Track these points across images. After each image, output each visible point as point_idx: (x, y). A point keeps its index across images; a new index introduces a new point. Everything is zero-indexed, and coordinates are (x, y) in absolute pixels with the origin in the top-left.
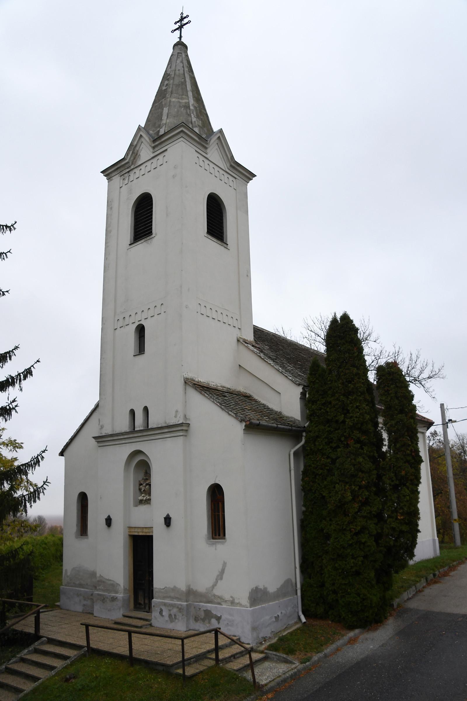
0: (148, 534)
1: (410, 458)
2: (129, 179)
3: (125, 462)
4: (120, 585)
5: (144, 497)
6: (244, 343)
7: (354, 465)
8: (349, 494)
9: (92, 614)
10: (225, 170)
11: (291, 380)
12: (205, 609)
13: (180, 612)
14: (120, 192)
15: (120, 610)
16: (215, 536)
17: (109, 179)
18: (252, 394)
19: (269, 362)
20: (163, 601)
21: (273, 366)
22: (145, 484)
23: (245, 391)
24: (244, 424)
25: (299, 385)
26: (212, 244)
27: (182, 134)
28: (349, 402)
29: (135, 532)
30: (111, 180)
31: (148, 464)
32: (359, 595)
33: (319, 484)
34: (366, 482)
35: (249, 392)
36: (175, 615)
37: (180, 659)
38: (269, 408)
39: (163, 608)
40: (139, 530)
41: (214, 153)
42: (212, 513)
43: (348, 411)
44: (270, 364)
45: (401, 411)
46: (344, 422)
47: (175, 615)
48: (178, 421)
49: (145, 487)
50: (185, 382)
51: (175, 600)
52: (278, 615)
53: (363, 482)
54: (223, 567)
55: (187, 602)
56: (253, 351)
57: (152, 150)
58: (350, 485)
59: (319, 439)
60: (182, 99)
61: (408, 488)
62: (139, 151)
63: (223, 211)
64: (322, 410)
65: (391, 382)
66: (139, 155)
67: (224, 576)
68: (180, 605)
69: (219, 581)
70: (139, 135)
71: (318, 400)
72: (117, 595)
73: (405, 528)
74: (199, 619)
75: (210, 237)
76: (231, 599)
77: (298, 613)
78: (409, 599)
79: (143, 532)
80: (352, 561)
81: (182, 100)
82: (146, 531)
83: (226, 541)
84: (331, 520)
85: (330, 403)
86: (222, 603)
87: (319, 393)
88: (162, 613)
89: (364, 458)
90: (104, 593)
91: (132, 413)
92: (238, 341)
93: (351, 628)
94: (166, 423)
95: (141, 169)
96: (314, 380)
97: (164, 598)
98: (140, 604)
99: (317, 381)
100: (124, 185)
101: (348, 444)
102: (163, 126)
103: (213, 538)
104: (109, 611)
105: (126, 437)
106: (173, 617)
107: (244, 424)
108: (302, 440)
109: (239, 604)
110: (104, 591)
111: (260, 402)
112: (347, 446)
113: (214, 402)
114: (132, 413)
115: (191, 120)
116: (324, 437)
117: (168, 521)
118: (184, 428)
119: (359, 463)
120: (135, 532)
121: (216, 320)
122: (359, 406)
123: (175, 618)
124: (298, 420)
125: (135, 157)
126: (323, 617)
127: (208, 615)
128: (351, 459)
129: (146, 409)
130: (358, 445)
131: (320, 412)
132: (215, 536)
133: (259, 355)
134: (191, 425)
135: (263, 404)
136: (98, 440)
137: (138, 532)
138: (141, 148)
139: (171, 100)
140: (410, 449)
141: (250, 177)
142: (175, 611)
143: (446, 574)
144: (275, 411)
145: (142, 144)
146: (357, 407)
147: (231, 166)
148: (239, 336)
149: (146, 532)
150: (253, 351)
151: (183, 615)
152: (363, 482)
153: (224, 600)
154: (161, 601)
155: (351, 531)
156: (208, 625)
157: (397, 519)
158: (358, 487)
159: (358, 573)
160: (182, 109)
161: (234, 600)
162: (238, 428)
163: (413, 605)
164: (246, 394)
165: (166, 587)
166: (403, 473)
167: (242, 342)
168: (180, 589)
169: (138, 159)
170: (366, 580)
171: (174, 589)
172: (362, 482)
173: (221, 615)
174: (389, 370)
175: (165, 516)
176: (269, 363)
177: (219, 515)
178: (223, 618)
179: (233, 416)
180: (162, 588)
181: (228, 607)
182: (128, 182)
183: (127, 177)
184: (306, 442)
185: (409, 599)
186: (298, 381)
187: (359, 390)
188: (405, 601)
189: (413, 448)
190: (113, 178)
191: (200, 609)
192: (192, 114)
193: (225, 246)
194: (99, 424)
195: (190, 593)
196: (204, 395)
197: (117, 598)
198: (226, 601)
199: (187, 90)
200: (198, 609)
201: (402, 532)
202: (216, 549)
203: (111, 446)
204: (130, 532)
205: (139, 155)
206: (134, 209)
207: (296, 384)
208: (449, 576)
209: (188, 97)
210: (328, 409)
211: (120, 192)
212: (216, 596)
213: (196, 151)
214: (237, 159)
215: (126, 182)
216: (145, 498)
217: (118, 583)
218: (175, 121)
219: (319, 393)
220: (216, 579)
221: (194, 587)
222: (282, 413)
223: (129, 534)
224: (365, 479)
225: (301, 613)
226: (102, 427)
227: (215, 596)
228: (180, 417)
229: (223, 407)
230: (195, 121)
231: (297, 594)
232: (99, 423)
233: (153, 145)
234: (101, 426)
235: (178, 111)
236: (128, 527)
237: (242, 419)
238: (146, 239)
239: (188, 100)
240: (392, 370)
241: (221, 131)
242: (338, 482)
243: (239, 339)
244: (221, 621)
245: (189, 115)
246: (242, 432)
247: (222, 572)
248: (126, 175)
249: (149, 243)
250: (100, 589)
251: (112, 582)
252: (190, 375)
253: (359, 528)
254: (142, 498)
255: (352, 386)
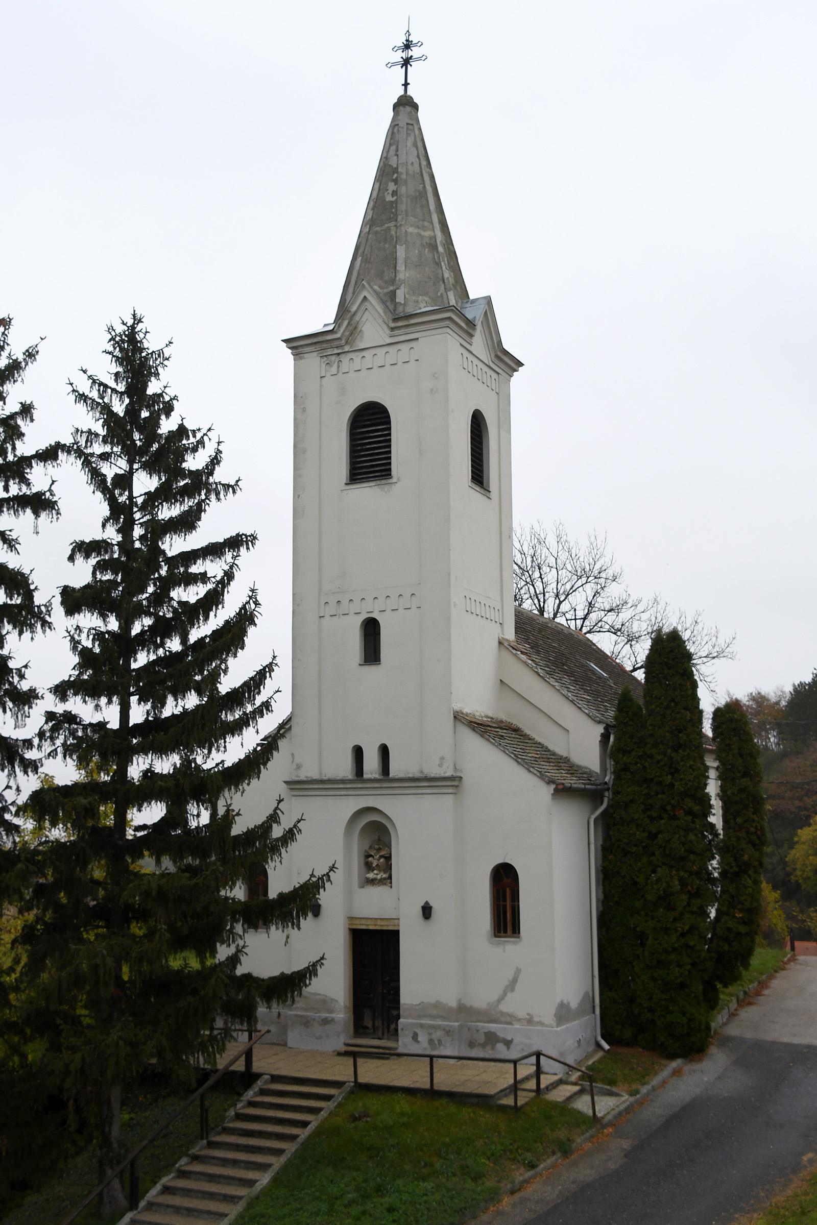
0: (391, 928)
1: (754, 838)
2: (338, 367)
3: (347, 821)
4: (337, 1001)
5: (377, 874)
6: (511, 649)
7: (683, 844)
8: (677, 882)
9: (285, 1045)
10: (487, 363)
11: (588, 715)
12: (486, 1031)
13: (448, 1036)
14: (321, 386)
15: (338, 1036)
16: (498, 932)
17: (296, 355)
18: (520, 726)
19: (551, 683)
20: (419, 1021)
21: (558, 690)
22: (378, 856)
23: (509, 720)
24: (553, 786)
25: (599, 722)
26: (475, 495)
27: (448, 322)
28: (679, 759)
29: (361, 925)
30: (301, 358)
31: (387, 827)
32: (684, 1014)
33: (630, 866)
34: (698, 866)
35: (516, 722)
36: (439, 1041)
37: (512, 1081)
38: (549, 751)
39: (419, 1031)
40: (369, 922)
41: (479, 343)
42: (494, 902)
43: (677, 771)
44: (554, 686)
45: (745, 774)
46: (672, 785)
47: (439, 1041)
48: (445, 772)
49: (379, 860)
50: (455, 717)
51: (438, 1020)
52: (580, 1039)
53: (695, 868)
54: (515, 974)
55: (458, 1022)
56: (525, 663)
57: (388, 332)
58: (677, 870)
59: (633, 805)
60: (424, 228)
61: (750, 877)
62: (361, 324)
63: (483, 433)
64: (639, 765)
65: (733, 733)
66: (360, 331)
67: (518, 986)
68: (448, 1025)
69: (509, 994)
70: (362, 297)
71: (633, 750)
72: (333, 1015)
73: (743, 929)
74: (477, 1044)
75: (474, 486)
76: (528, 1017)
77: (596, 1038)
78: (725, 1024)
79: (376, 925)
80: (677, 969)
81: (424, 231)
82: (382, 924)
83: (520, 941)
84: (646, 915)
85: (651, 756)
86: (514, 1023)
87: (633, 741)
88: (417, 1038)
89: (696, 835)
90: (308, 1014)
91: (358, 752)
92: (500, 643)
93: (672, 1057)
94: (422, 772)
95: (364, 357)
96: (625, 721)
97: (419, 1017)
98: (366, 1028)
99: (631, 723)
100: (328, 374)
101: (675, 815)
102: (401, 284)
103: (496, 936)
104: (317, 1038)
105: (348, 786)
106: (436, 1042)
107: (553, 786)
108: (602, 803)
109: (540, 1023)
110: (306, 1010)
111: (534, 739)
112: (674, 818)
113: (506, 753)
114: (358, 752)
115: (443, 274)
116: (639, 802)
117: (427, 911)
118: (456, 783)
119: (691, 842)
120: (361, 925)
121: (479, 617)
122: (693, 765)
123: (439, 1044)
124: (596, 773)
125: (352, 333)
126: (631, 1043)
127: (492, 1039)
128: (680, 836)
129: (384, 751)
130: (689, 818)
131: (635, 767)
132: (498, 932)
133: (536, 670)
134: (464, 779)
135: (539, 743)
136: (292, 787)
137: (368, 925)
138: (364, 319)
139: (407, 230)
140: (754, 825)
141: (387, 467)
142: (439, 1034)
143: (758, 993)
144: (559, 755)
145: (367, 311)
146: (691, 767)
147: (497, 357)
148: (501, 636)
149: (381, 926)
150: (525, 663)
151: (452, 1040)
152: (695, 868)
153: (515, 1018)
154: (414, 1021)
155: (676, 931)
156: (490, 1052)
157: (734, 917)
158: (688, 873)
159: (682, 986)
160: (427, 250)
161: (532, 1017)
162: (546, 791)
163: (732, 1030)
164: (512, 724)
165: (423, 1002)
166: (746, 857)
167: (508, 647)
168: (447, 1004)
169: (358, 337)
170: (693, 995)
171: (438, 1005)
172: (692, 866)
173: (512, 1039)
174: (731, 715)
175: (422, 904)
176: (552, 685)
177: (506, 905)
178: (515, 1041)
179: (535, 774)
180: (415, 1003)
181: (523, 1027)
182: (338, 372)
183: (335, 362)
184: (608, 805)
185: (725, 1024)
186: (598, 717)
187: (694, 743)
188: (720, 1027)
189: (758, 825)
190: (306, 355)
191: (478, 1031)
192: (443, 264)
193: (487, 494)
194: (293, 762)
195: (463, 1009)
196: (488, 740)
197: (333, 1020)
198: (519, 1020)
199: (430, 209)
200: (475, 1032)
201: (739, 934)
202: (504, 951)
203: (318, 798)
204: (353, 924)
205: (360, 331)
206: (351, 421)
207: (595, 721)
208: (764, 995)
209: (433, 225)
210: (647, 764)
211: (321, 386)
212: (504, 1013)
213: (461, 344)
214: (506, 346)
215: (334, 370)
216: (379, 877)
217: (333, 998)
218: (418, 276)
219: (633, 741)
220: (504, 991)
221: (468, 1003)
222: (571, 760)
223: (350, 927)
224: (696, 863)
225: (599, 1038)
226: (299, 767)
227: (502, 1013)
228: (448, 768)
229: (520, 760)
230: (448, 278)
231: (594, 1012)
232: (293, 759)
233: (393, 325)
234: (297, 765)
235: (420, 255)
236: (348, 918)
237: (550, 780)
238: (378, 482)
239: (434, 231)
240: (735, 716)
241: (488, 300)
242: (661, 864)
243: (502, 641)
244: (512, 1046)
245: (438, 264)
246: (550, 797)
247: (514, 982)
248: (333, 358)
249: (386, 490)
250: (298, 1008)
251: (322, 997)
252: (459, 706)
253: (687, 927)
254: (375, 876)
255: (685, 738)
